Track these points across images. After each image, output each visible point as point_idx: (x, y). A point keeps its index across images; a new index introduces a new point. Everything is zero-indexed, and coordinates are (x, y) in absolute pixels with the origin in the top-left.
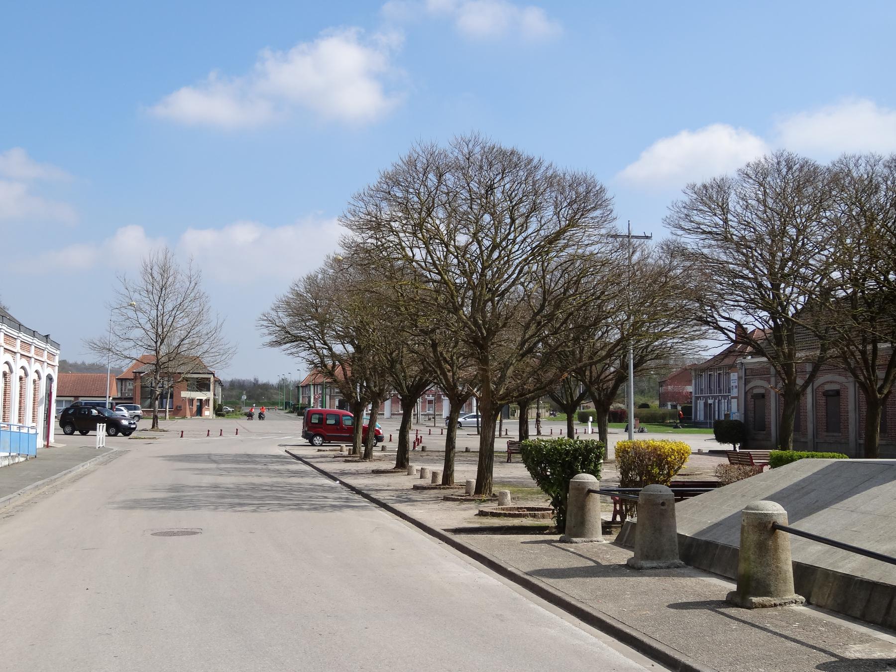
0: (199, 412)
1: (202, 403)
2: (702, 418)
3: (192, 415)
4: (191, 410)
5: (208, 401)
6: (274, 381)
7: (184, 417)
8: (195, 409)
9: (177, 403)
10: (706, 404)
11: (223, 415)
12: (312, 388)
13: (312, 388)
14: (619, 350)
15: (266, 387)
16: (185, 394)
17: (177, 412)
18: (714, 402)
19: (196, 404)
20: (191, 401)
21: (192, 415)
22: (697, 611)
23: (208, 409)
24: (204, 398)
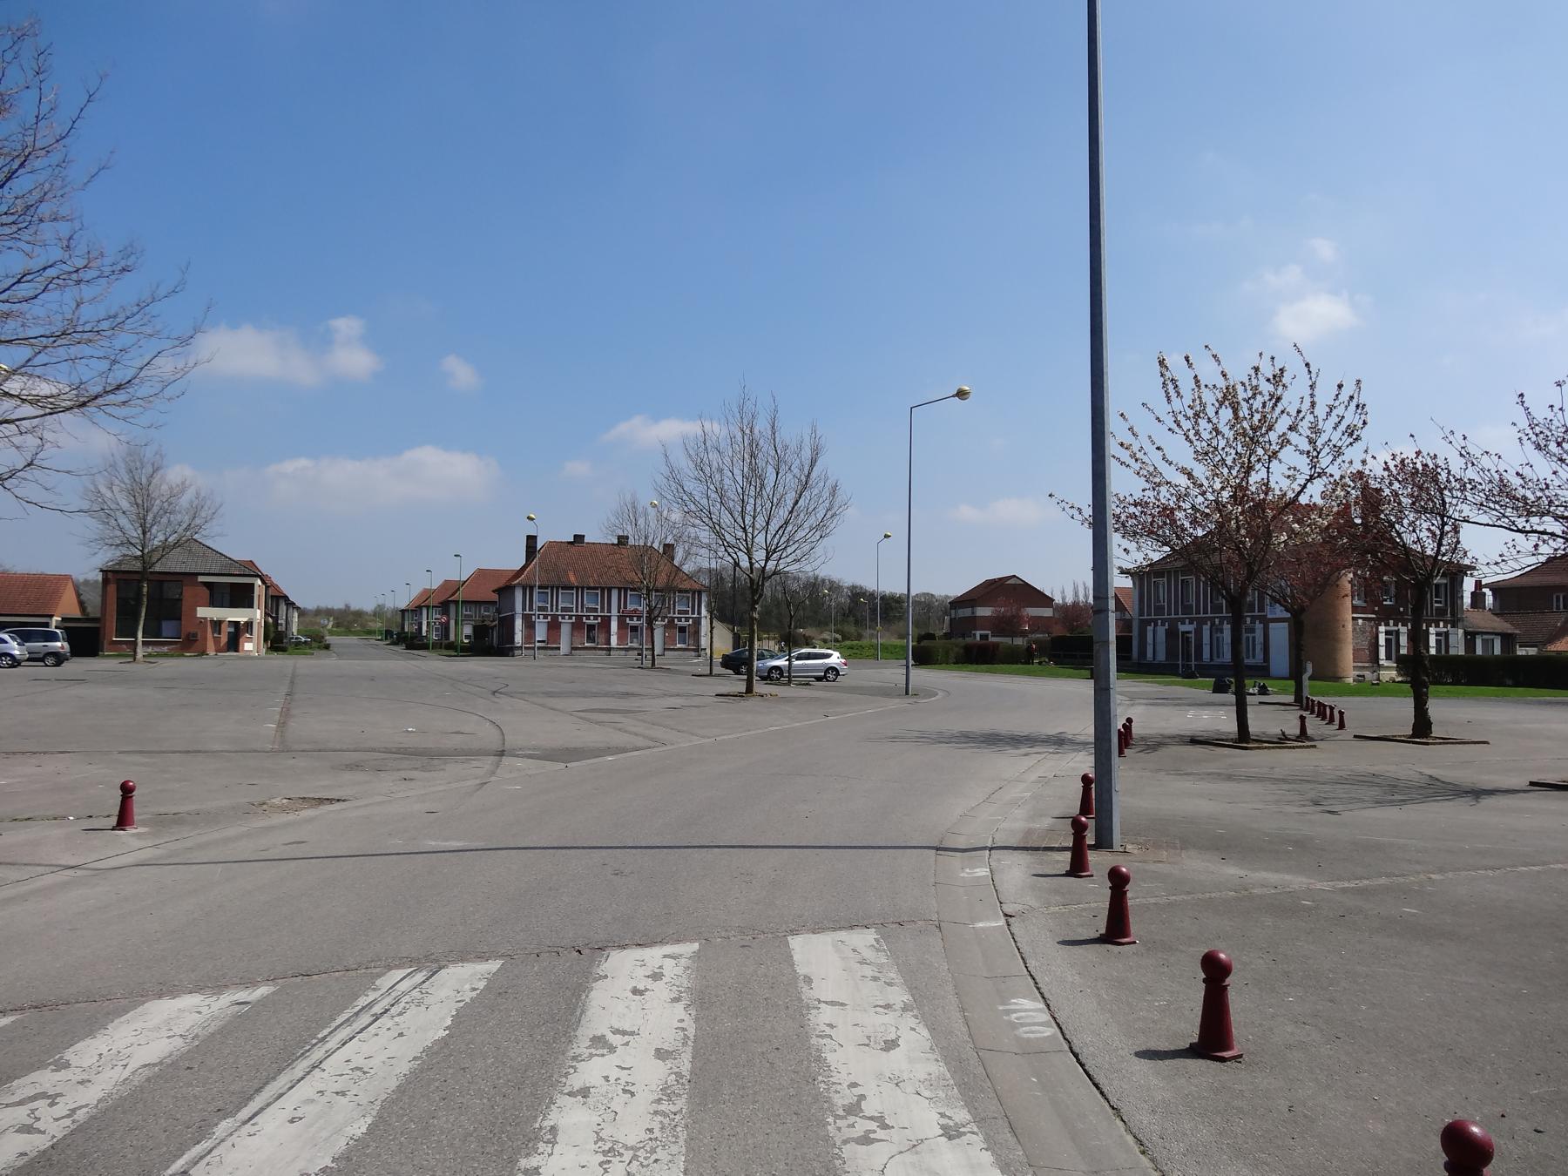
0: (234, 644)
1: (239, 632)
2: (1161, 657)
3: (218, 650)
4: (217, 641)
5: (249, 625)
6: (368, 606)
7: (202, 653)
8: (224, 639)
9: (187, 627)
10: (1172, 634)
11: (284, 650)
12: (615, 594)
13: (615, 594)
14: (530, 625)
15: (359, 614)
16: (204, 612)
17: (190, 643)
18: (1199, 632)
19: (226, 630)
20: (217, 625)
21: (218, 650)
22: (1105, 904)
23: (250, 640)
24: (243, 620)
